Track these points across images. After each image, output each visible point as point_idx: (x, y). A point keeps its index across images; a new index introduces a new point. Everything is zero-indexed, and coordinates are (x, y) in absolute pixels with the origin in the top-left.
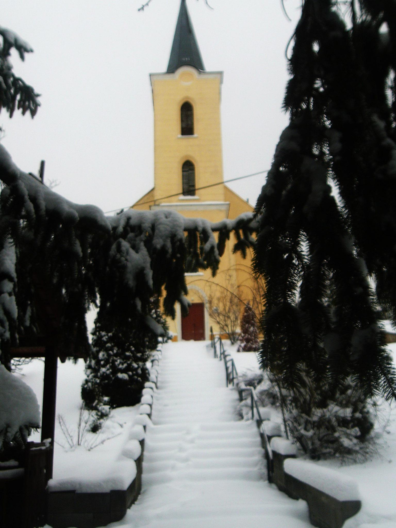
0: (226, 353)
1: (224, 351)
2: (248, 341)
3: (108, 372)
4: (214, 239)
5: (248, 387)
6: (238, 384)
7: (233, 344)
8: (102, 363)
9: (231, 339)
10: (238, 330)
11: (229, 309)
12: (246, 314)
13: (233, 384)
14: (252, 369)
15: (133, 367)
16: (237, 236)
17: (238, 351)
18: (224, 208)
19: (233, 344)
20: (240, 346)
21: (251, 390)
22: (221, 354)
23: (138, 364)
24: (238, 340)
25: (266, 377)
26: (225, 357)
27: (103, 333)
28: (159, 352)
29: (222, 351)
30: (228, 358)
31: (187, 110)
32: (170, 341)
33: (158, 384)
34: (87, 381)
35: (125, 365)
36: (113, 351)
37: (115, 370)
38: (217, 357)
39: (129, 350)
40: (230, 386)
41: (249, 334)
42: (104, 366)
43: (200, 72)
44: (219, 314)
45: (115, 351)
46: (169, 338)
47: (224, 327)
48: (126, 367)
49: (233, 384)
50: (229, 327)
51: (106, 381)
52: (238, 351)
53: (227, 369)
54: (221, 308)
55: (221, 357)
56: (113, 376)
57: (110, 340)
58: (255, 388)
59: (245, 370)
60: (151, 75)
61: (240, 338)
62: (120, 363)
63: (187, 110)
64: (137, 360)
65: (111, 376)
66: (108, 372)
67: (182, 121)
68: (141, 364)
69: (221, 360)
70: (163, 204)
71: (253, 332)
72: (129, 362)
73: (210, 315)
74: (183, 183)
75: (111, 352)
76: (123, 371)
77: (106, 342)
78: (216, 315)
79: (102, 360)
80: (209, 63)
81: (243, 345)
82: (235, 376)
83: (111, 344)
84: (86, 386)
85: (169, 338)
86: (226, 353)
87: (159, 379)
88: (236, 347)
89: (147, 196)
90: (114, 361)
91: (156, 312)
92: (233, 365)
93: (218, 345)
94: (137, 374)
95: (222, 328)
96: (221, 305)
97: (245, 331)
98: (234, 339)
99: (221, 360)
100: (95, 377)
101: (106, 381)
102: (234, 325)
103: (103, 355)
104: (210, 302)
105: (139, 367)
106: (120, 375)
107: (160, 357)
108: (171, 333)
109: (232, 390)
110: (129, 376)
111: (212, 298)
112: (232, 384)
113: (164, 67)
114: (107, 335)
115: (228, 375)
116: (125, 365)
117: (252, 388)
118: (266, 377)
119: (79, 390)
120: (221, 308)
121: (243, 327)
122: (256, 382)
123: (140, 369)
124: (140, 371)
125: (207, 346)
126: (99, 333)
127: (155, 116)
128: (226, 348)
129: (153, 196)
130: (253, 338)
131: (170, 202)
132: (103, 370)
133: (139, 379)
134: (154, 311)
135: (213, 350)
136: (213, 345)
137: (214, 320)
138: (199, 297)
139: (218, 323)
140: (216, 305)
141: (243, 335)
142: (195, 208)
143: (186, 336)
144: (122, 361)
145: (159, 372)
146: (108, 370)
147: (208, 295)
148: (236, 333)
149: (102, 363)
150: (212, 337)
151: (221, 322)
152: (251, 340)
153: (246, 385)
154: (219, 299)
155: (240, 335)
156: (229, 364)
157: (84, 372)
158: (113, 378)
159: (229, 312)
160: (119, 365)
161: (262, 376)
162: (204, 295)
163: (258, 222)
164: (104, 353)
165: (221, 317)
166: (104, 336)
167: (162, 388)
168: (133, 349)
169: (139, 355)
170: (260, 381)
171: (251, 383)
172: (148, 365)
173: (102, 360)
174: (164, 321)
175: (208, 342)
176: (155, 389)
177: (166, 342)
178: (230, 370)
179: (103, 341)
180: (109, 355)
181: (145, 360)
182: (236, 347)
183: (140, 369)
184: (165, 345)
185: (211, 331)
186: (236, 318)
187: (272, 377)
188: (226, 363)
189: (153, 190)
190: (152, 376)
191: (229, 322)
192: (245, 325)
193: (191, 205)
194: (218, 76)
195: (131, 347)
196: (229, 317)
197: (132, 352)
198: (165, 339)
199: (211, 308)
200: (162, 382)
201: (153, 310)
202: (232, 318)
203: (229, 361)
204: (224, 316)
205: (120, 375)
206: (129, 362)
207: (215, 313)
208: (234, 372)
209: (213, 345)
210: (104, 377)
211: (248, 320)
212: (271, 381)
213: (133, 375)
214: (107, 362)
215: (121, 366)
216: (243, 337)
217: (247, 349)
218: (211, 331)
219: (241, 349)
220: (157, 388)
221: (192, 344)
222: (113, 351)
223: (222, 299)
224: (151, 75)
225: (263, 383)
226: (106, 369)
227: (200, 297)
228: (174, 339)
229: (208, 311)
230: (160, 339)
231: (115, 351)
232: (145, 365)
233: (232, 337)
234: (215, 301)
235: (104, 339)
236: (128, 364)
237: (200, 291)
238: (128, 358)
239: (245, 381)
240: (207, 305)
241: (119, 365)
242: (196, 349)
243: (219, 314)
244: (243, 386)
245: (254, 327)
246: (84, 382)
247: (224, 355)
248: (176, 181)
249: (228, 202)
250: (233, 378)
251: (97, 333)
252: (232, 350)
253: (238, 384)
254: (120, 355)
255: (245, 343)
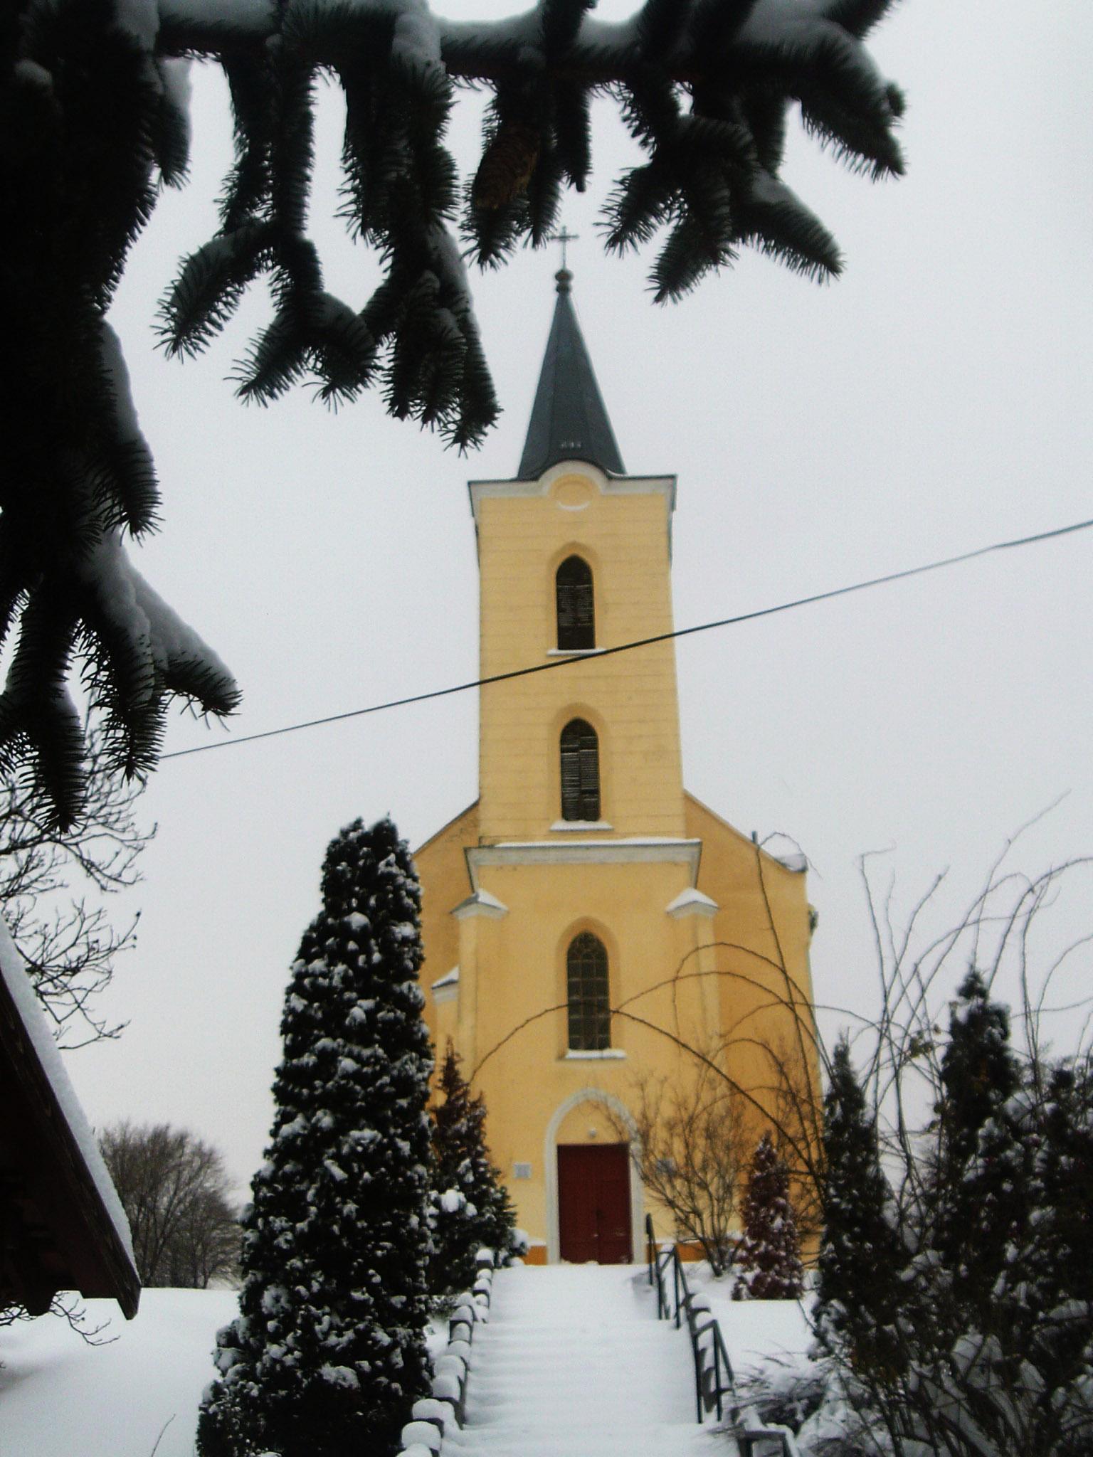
0: (695, 1303)
1: (689, 1296)
2: (767, 1261)
3: (289, 1360)
4: (419, 42)
5: (772, 1427)
6: (734, 1413)
7: (717, 1273)
8: (271, 1325)
9: (710, 1259)
10: (735, 1229)
11: (705, 1161)
12: (758, 1174)
13: (719, 1411)
14: (783, 1359)
15: (376, 1342)
16: (650, 115)
17: (737, 1296)
18: (684, 856)
19: (717, 1273)
20: (742, 1280)
21: (782, 1437)
22: (678, 1306)
23: (392, 1335)
24: (732, 1261)
25: (835, 1389)
26: (693, 1313)
27: (279, 1222)
28: (481, 1297)
29: (682, 1296)
30: (701, 1319)
31: (574, 581)
32: (517, 1261)
33: (469, 1407)
34: (217, 1390)
35: (349, 1335)
36: (309, 1287)
37: (314, 1353)
38: (667, 1317)
39: (363, 1281)
40: (710, 1419)
41: (771, 1242)
42: (276, 1338)
43: (610, 478)
44: (672, 1174)
45: (316, 1286)
46: (517, 1252)
47: (687, 1217)
48: (350, 1342)
49: (719, 1411)
50: (706, 1216)
51: (283, 1393)
52: (737, 1296)
53: (698, 1355)
54: (678, 1158)
55: (677, 1315)
56: (305, 1375)
57: (302, 1244)
58: (796, 1429)
59: (759, 1364)
60: (470, 484)
61: (742, 1253)
62: (332, 1327)
63: (574, 581)
64: (389, 1318)
65: (299, 1374)
66: (289, 1360)
67: (560, 610)
68: (402, 1331)
69: (678, 1325)
70: (501, 845)
71: (781, 1233)
72: (361, 1326)
73: (645, 1178)
74: (564, 785)
75: (301, 1289)
76: (339, 1358)
77: (288, 1255)
78: (664, 1179)
79: (271, 1317)
80: (634, 459)
81: (749, 1276)
82: (724, 1383)
83: (302, 1260)
84: (213, 1409)
85: (517, 1252)
86: (695, 1303)
87: (470, 1389)
88: (728, 1284)
89: (460, 825)
90: (311, 1320)
91: (475, 1166)
92: (718, 1342)
93: (668, 1274)
94: (389, 1370)
95: (683, 1221)
96: (678, 1146)
97: (757, 1228)
98: (722, 1254)
99: (678, 1325)
100: (246, 1375)
101: (283, 1393)
102: (722, 1212)
103: (277, 1299)
104: (645, 1137)
105: (395, 1344)
106: (329, 1372)
107: (481, 1312)
108: (522, 1234)
109: (714, 1432)
110: (360, 1373)
111: (649, 1126)
112: (714, 1413)
113: (512, 472)
114: (292, 1229)
115: (701, 1379)
116: (349, 1335)
117: (785, 1429)
118: (835, 1389)
119: (194, 1424)
120: (678, 1158)
121: (747, 1220)
122: (800, 1406)
123: (398, 1350)
124: (398, 1360)
125: (636, 1280)
126: (267, 1223)
127: (482, 580)
128: (693, 1284)
129: (476, 823)
130: (783, 1254)
131: (525, 837)
132: (274, 1350)
133: (396, 1385)
134: (467, 1161)
135: (654, 1293)
136: (656, 1278)
137: (655, 1194)
138: (609, 1119)
139: (671, 1204)
140: (661, 1146)
141: (749, 1243)
142: (597, 855)
143: (573, 1251)
144: (337, 1320)
145: (474, 1362)
146: (290, 1351)
147: (637, 1114)
148: (728, 1240)
149: (271, 1325)
150: (653, 1252)
151: (680, 1203)
152: (778, 1260)
153: (765, 1421)
154: (670, 1126)
155: (741, 1243)
156: (706, 1339)
157: (211, 1359)
158: (305, 1382)
159: (704, 1169)
160: (326, 1334)
161: (820, 1383)
162: (625, 1114)
163: (836, 40)
164: (281, 1291)
165: (678, 1183)
166: (283, 1230)
167: (482, 1421)
168: (377, 1279)
169: (398, 1300)
170: (814, 1404)
171: (782, 1411)
172: (435, 1337)
173: (271, 1317)
174: (499, 1195)
175: (640, 1267)
176: (451, 1425)
177: (506, 1263)
178: (708, 1361)
179: (278, 1248)
180: (295, 1299)
181: (418, 1321)
182: (728, 1284)
183: (398, 1350)
184: (502, 1273)
185: (649, 1230)
186: (728, 1189)
187: (858, 1389)
188: (695, 1338)
189: (476, 805)
190: (446, 1380)
191: (702, 1203)
192: (756, 1209)
193: (588, 847)
194: (663, 486)
195: (371, 1271)
196: (704, 1186)
197: (372, 1289)
198: (503, 1254)
199: (646, 1153)
200: (482, 1400)
201: (464, 1159)
202: (712, 1189)
203: (704, 1328)
204: (688, 1180)
205: (329, 1372)
206: (361, 1326)
207: (660, 1174)
208: (722, 1368)
209: (656, 1278)
210: (278, 1376)
211: (765, 1190)
212: (857, 1403)
213: (376, 1372)
214: (287, 1322)
215: (333, 1339)
216: (750, 1250)
217: (765, 1290)
218: (649, 1230)
219: (745, 1291)
220: (461, 1419)
221: (591, 1270)
222: (309, 1287)
223: (679, 1129)
224: (470, 484)
225: (824, 1410)
226: (284, 1349)
227: (614, 1121)
228: (537, 1257)
229: (636, 1163)
230: (484, 1253)
231: (316, 1286)
232: (419, 1336)
233: (716, 1252)
234: (660, 1133)
235: (281, 1241)
236: (357, 1332)
237: (611, 1101)
238: (358, 1310)
239: (763, 1403)
240: (635, 1147)
241: (326, 1334)
242: (603, 1288)
243: (672, 1174)
244: (754, 1423)
245: (784, 1218)
246: (210, 1394)
247: (689, 1310)
248: (543, 772)
249: (696, 840)
250: (720, 1391)
251: (260, 1222)
252: (714, 1294)
253: (734, 1413)
254: (331, 1299)
255: (757, 1271)
